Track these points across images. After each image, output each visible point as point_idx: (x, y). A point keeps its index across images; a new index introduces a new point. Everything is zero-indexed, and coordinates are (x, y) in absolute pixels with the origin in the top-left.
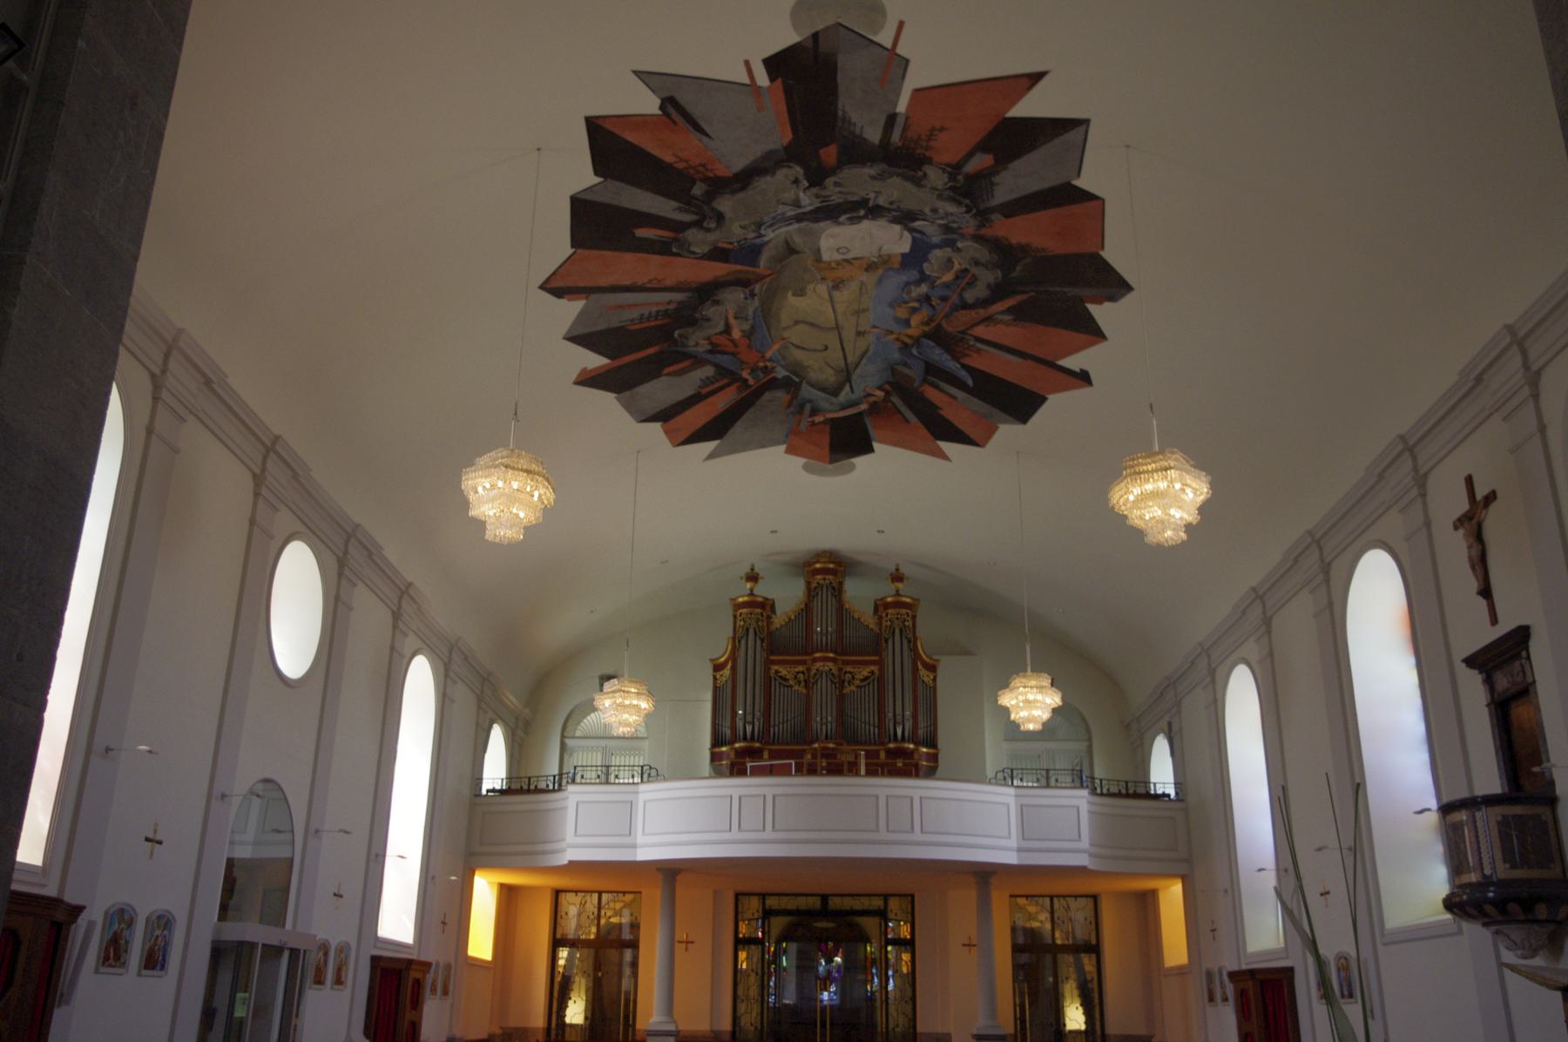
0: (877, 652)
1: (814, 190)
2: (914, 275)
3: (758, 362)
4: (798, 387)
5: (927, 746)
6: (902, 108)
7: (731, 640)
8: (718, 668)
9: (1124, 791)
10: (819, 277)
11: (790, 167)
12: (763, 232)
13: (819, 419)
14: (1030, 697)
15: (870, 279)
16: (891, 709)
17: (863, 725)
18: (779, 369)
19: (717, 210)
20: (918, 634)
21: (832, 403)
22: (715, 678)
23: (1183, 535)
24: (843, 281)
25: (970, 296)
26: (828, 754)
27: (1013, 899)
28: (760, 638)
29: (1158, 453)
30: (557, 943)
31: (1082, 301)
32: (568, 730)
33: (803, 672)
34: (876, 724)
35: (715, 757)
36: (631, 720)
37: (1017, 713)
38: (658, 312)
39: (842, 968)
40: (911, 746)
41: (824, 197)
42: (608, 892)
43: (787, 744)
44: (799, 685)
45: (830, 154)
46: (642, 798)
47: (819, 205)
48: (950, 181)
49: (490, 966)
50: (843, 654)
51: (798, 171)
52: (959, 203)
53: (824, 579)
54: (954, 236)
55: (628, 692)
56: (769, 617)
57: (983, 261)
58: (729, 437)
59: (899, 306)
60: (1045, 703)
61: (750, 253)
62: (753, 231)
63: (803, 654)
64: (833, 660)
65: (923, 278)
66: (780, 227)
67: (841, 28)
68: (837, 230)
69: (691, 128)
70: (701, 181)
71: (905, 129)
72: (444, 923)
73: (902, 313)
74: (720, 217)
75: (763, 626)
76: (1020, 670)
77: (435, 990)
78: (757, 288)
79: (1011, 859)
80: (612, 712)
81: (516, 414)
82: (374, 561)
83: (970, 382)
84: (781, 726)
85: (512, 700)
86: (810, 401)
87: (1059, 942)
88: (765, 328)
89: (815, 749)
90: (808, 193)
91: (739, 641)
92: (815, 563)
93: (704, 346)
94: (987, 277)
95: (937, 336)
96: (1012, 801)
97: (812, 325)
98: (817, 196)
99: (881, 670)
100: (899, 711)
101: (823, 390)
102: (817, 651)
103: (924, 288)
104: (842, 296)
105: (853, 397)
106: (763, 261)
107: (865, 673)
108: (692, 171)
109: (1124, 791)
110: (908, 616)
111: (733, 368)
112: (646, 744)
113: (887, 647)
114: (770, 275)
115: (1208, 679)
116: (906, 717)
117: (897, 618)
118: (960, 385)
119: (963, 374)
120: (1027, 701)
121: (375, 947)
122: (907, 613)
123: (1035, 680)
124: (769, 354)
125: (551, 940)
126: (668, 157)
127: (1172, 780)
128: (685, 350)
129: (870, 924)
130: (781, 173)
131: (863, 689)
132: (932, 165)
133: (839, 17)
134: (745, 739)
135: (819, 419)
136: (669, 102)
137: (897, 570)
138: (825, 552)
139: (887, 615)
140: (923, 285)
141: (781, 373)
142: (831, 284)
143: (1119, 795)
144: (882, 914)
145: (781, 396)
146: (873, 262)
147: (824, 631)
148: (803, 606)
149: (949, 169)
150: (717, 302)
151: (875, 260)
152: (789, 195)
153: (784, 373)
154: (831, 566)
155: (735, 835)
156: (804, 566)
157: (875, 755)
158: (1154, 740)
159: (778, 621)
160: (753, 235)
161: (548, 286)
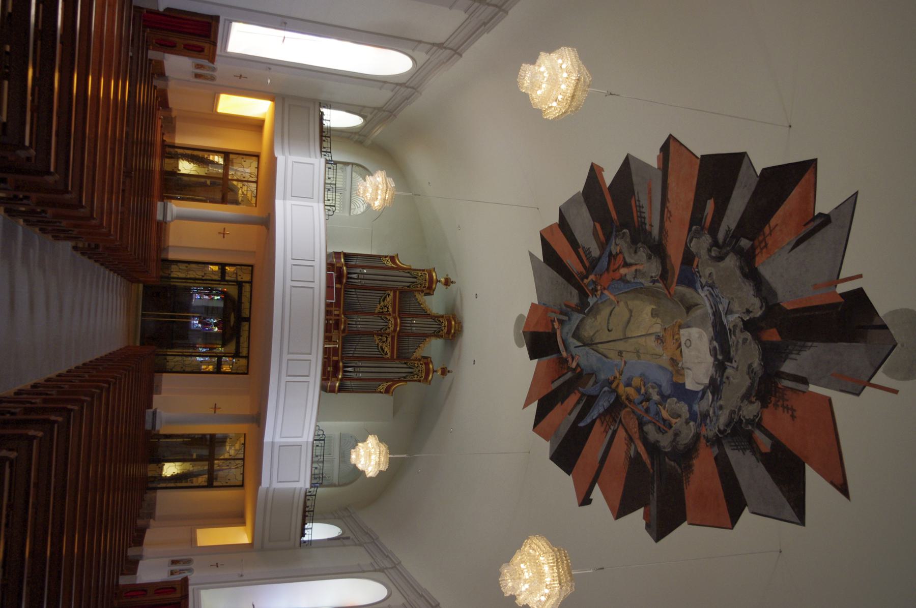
0: (399, 358)
1: (741, 324)
2: (667, 390)
3: (601, 285)
4: (581, 311)
5: (339, 386)
6: (812, 388)
7: (409, 267)
8: (392, 259)
9: (307, 509)
10: (667, 327)
11: (761, 308)
12: (706, 288)
13: (556, 325)
14: (373, 457)
15: (665, 361)
16: (363, 365)
17: (354, 347)
18: (595, 299)
19: (726, 256)
20: (408, 383)
21: (567, 333)
22: (386, 257)
23: (508, 594)
24: (663, 343)
25: (649, 429)
26: (337, 324)
27: (243, 436)
28: (410, 285)
29: (571, 576)
30: (226, 154)
31: (645, 504)
32: (357, 167)
33: (388, 311)
34: (355, 355)
35: (337, 254)
36: (367, 194)
37: (363, 448)
38: (644, 218)
39: (212, 331)
40: (340, 377)
41: (734, 332)
42: (257, 187)
43: (345, 299)
44: (380, 308)
45: (772, 335)
46: (315, 205)
47: (727, 327)
48: (746, 420)
49: (214, 111)
50: (398, 336)
51: (758, 313)
52: (728, 425)
53: (445, 326)
54: (699, 420)
55: (386, 193)
56: (422, 291)
57: (678, 439)
58: (545, 266)
59: (641, 380)
60: (369, 466)
61: (689, 279)
62: (706, 282)
63: (399, 311)
64: (395, 330)
65: (664, 397)
66: (709, 300)
67: (891, 346)
68: (706, 339)
69: (801, 236)
70: (753, 245)
71: (792, 389)
72: (241, 77)
73: (636, 382)
74: (720, 258)
75: (417, 287)
76: (391, 450)
77: (198, 68)
78: (660, 285)
79: (267, 438)
80: (373, 182)
81: (611, 94)
82: (480, 26)
83: (581, 424)
84: (355, 296)
85: (378, 132)
86: (569, 319)
87: (216, 462)
88: (627, 290)
89: (341, 316)
90: (738, 320)
91: (409, 272)
92: (455, 321)
93: (614, 249)
94: (665, 442)
95: (618, 405)
96: (304, 439)
97: (628, 322)
98: (735, 326)
99: (387, 360)
100: (362, 370)
101: (578, 328)
102: (401, 320)
103: (656, 397)
104: (651, 342)
105: (572, 348)
106: (682, 289)
107: (386, 349)
108: (761, 238)
109: (307, 509)
110: (420, 377)
111: (597, 269)
112: (347, 215)
113: (402, 364)
114: (669, 293)
115: (377, 567)
116: (358, 374)
117: (419, 371)
118: (580, 417)
119: (588, 420)
120: (370, 455)
121: (225, 20)
122: (422, 377)
123: (384, 460)
124: (606, 292)
125: (230, 151)
126: (773, 222)
127: (313, 539)
128: (613, 237)
129: (232, 347)
130: (756, 302)
131: (376, 348)
132: (761, 408)
133: (902, 345)
134: (348, 273)
135: (556, 325)
136: (826, 220)
137: (449, 372)
138: (462, 327)
139: (421, 364)
140: (658, 397)
141: (592, 300)
142: (661, 335)
143: (305, 506)
144: (237, 355)
145: (575, 301)
146: (678, 364)
147: (412, 325)
148: (428, 312)
149: (757, 420)
150: (649, 258)
151: (680, 365)
152: (736, 306)
153: (591, 304)
154: (453, 331)
155: (290, 262)
156: (453, 315)
157: (336, 353)
158: (340, 528)
159: (420, 297)
160: (704, 283)
161: (671, 141)
